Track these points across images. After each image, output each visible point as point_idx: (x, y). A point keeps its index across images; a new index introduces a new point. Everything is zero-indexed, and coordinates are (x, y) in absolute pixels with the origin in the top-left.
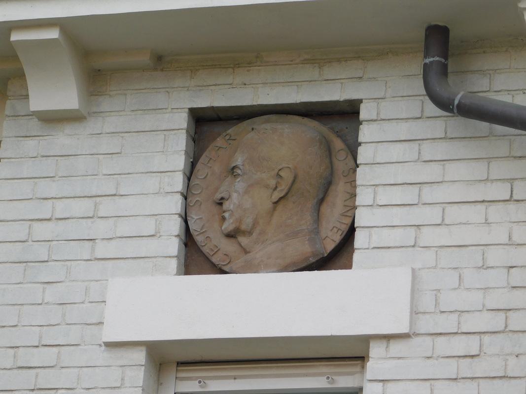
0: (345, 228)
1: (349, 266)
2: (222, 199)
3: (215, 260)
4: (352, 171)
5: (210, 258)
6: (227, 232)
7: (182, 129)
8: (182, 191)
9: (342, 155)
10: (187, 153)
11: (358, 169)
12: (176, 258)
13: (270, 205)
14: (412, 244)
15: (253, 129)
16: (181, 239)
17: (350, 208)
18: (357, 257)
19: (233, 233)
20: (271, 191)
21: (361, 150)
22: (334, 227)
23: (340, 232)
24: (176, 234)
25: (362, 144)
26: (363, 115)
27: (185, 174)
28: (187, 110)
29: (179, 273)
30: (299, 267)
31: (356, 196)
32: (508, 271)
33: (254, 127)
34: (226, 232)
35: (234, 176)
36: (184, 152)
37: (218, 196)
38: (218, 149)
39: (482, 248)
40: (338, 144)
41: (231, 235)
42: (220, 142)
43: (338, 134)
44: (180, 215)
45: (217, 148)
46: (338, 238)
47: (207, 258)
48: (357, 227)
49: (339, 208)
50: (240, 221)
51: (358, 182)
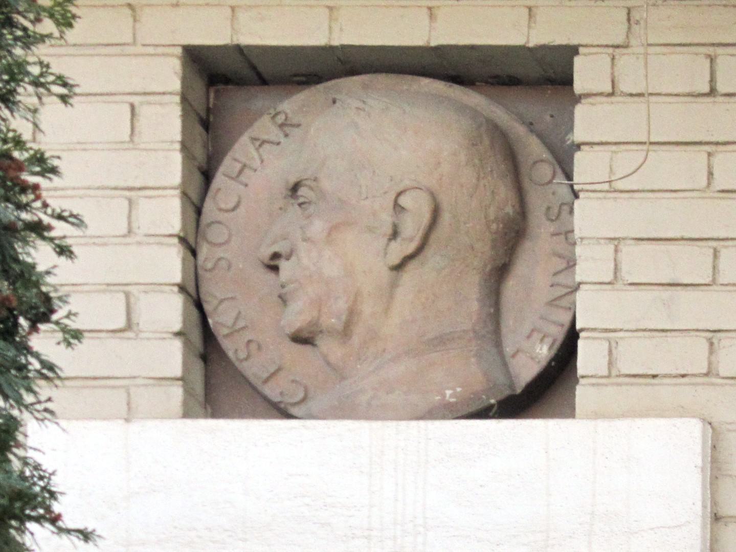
0: (559, 334)
1: (568, 411)
2: (276, 256)
3: (272, 391)
4: (566, 208)
5: (260, 387)
6: (293, 330)
7: (171, 93)
8: (182, 234)
9: (545, 171)
10: (185, 147)
11: (577, 204)
12: (180, 383)
13: (386, 275)
14: (705, 371)
15: (334, 102)
16: (187, 344)
17: (569, 290)
18: (583, 394)
19: (305, 334)
20: (385, 240)
21: (580, 159)
22: (533, 331)
23: (549, 340)
24: (177, 326)
25: (582, 147)
26: (579, 86)
27: (185, 195)
28: (179, 51)
29: (187, 414)
30: (464, 413)
31: (575, 265)
32: (178, 379)
33: (338, 97)
34: (290, 330)
35: (300, 205)
36: (178, 146)
37: (266, 252)
38: (260, 146)
39: (714, 244)
40: (533, 148)
41: (303, 339)
42: (264, 127)
43: (532, 127)
44: (182, 288)
45: (258, 143)
46: (544, 352)
47: (254, 388)
48: (582, 330)
49: (542, 290)
50: (318, 303)
51: (577, 233)
